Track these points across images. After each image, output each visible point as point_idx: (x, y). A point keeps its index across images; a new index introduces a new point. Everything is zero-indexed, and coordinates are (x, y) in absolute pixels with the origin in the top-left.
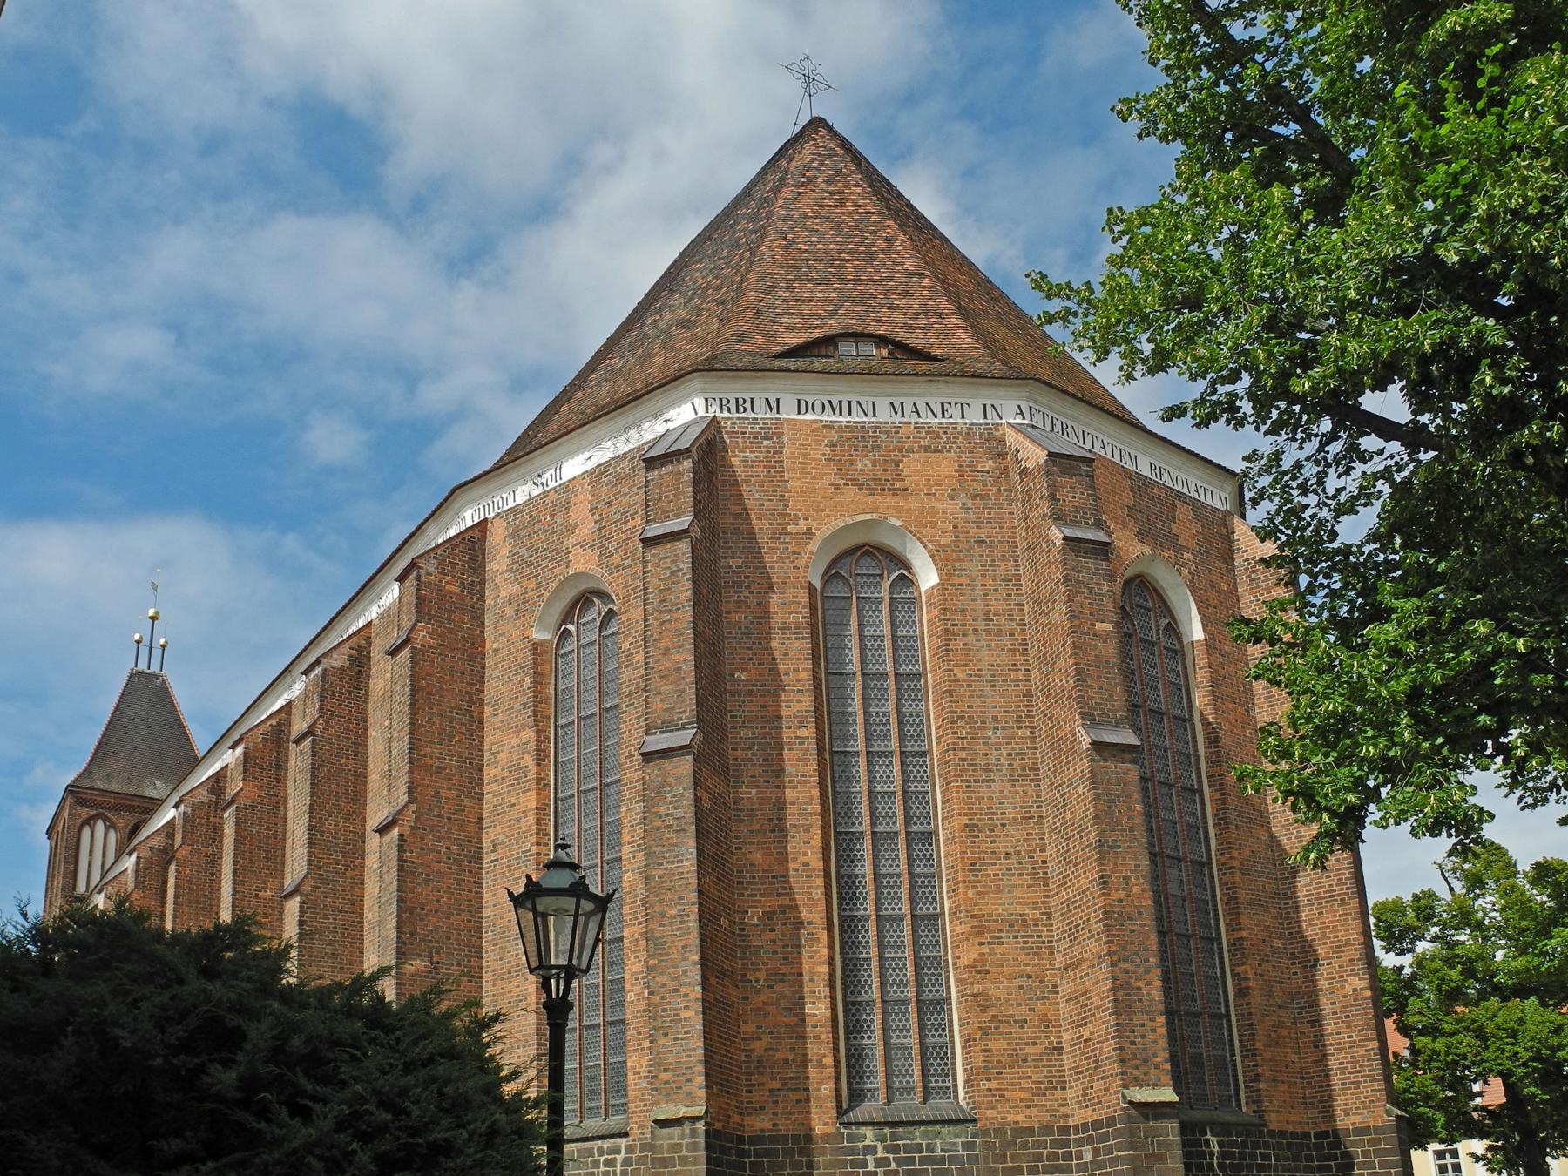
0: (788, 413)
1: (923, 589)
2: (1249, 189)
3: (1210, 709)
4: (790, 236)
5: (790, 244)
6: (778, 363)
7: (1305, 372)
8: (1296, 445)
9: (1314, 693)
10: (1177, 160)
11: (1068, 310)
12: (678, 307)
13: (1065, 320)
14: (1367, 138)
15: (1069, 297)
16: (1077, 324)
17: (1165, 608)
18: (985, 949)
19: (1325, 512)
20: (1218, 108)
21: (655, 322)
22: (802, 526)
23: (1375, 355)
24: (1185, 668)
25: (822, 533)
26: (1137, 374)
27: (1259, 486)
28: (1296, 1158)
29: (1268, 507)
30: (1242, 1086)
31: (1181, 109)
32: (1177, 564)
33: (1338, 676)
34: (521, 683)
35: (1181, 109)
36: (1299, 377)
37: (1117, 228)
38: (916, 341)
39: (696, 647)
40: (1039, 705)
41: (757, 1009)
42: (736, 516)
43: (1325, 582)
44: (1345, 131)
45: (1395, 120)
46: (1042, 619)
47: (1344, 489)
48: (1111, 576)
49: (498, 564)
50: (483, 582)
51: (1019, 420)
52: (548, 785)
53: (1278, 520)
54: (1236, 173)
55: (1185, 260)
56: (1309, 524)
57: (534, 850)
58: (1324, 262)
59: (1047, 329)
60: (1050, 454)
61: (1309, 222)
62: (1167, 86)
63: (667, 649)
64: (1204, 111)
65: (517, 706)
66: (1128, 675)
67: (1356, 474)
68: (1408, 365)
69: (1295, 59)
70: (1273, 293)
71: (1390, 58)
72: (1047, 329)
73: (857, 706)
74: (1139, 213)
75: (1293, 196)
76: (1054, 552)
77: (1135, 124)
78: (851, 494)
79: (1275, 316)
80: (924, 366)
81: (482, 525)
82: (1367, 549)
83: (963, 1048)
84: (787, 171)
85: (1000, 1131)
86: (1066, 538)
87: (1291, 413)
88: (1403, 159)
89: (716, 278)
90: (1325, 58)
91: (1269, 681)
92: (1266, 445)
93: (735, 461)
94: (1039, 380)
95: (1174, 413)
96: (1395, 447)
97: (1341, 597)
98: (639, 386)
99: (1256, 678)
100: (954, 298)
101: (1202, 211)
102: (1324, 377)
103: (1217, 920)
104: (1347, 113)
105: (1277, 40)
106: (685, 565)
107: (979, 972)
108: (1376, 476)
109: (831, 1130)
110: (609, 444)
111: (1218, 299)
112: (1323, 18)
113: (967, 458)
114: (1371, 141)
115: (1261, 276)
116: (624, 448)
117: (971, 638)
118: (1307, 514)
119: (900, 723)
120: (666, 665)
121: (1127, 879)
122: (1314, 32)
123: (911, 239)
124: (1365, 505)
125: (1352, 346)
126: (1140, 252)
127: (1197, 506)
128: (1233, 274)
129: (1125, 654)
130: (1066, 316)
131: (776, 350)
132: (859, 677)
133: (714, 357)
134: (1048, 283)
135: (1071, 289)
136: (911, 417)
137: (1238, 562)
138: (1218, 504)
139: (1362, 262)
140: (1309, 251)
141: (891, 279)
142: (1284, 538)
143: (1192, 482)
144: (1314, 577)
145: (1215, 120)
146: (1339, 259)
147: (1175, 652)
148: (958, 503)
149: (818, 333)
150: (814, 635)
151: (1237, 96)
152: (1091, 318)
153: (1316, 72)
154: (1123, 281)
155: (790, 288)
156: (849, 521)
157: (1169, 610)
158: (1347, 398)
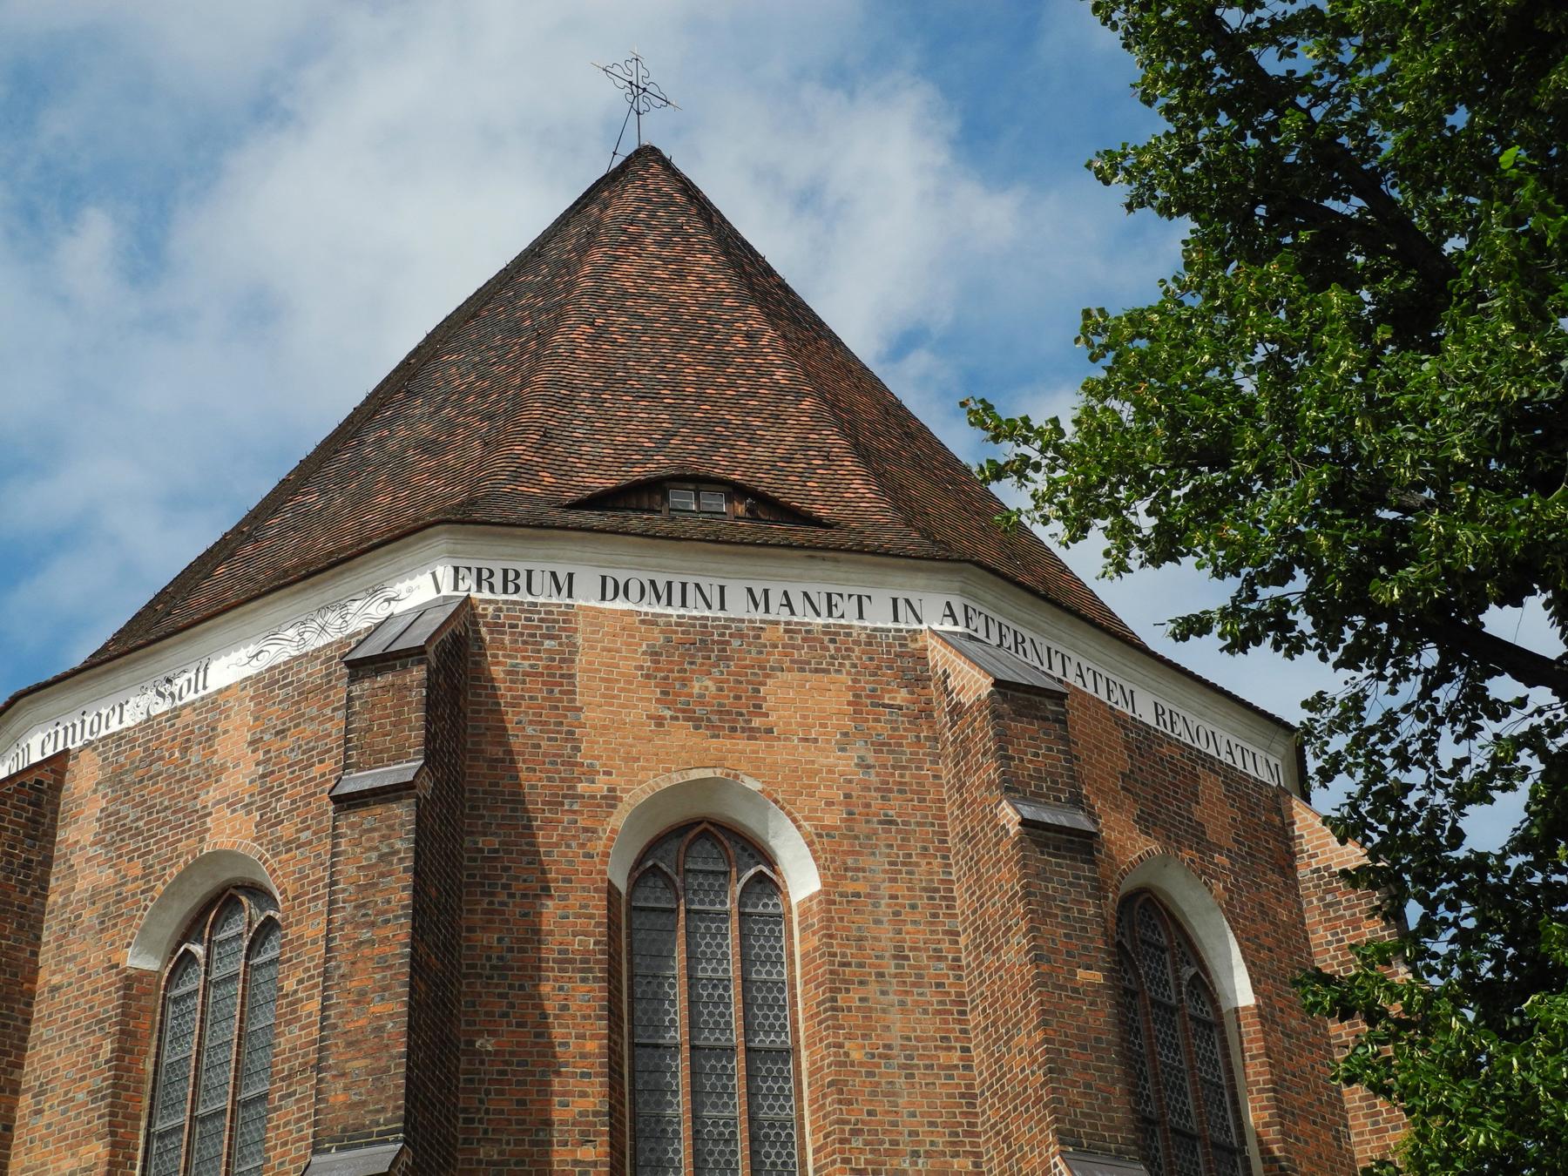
0: (586, 597)
2: (1295, 292)
3: (1272, 1134)
4: (599, 321)
5: (599, 335)
6: (573, 517)
7: (1392, 571)
8: (1384, 686)
9: (1450, 1114)
10: (1185, 242)
11: (1025, 460)
12: (419, 422)
13: (1021, 476)
14: (1468, 224)
15: (1026, 441)
16: (1040, 481)
17: (1189, 950)
19: (1439, 798)
20: (1243, 170)
21: (381, 439)
22: (601, 785)
23: (1500, 549)
24: (1227, 1056)
25: (635, 795)
26: (1133, 564)
27: (1331, 749)
29: (1345, 785)
31: (1188, 170)
32: (1205, 873)
33: (1489, 1083)
34: (95, 1051)
35: (1188, 170)
36: (1384, 578)
37: (1097, 340)
38: (789, 491)
39: (413, 989)
40: (988, 1113)
42: (494, 762)
43: (1451, 916)
44: (1432, 212)
45: (1507, 199)
46: (989, 959)
47: (1467, 761)
48: (1099, 890)
49: (79, 831)
50: (47, 862)
51: (948, 626)
53: (1365, 808)
54: (1273, 267)
55: (1201, 392)
56: (1415, 817)
58: (1413, 405)
59: (994, 487)
60: (998, 683)
61: (1385, 343)
62: (1168, 135)
63: (362, 993)
64: (1224, 174)
65: (81, 1096)
66: (1134, 1063)
67: (1485, 737)
68: (1554, 568)
69: (1356, 105)
70: (1336, 447)
71: (1495, 110)
72: (994, 487)
73: (681, 1106)
74: (1130, 320)
75: (1361, 303)
76: (1007, 845)
77: (1121, 190)
78: (681, 735)
79: (1341, 484)
80: (802, 534)
81: (58, 762)
82: (1513, 862)
84: (599, 223)
86: (1024, 823)
87: (1375, 637)
88: (1523, 260)
89: (481, 377)
90: (1400, 107)
91: (1371, 1086)
92: (1337, 683)
93: (497, 672)
94: (979, 564)
95: (1192, 627)
96: (1542, 695)
97: (1480, 944)
98: (348, 540)
99: (1350, 1081)
100: (849, 429)
101: (1223, 320)
102: (1423, 581)
104: (1436, 185)
105: (1328, 78)
106: (403, 845)
108: (1518, 742)
110: (291, 633)
111: (1253, 454)
112: (1394, 49)
113: (866, 683)
114: (1473, 227)
115: (1317, 421)
116: (315, 641)
117: (873, 988)
118: (1411, 799)
119: (753, 1139)
120: (359, 1021)
122: (1380, 68)
123: (784, 337)
124: (1504, 789)
125: (1464, 534)
126: (1133, 377)
127: (1232, 778)
128: (1274, 417)
129: (1127, 1024)
130: (1021, 468)
131: (571, 495)
132: (685, 1052)
133: (472, 502)
134: (995, 417)
135: (1030, 428)
136: (780, 614)
137: (1303, 873)
138: (1265, 776)
139: (1472, 407)
140: (1388, 385)
141: (754, 396)
142: (1377, 839)
143: (1223, 736)
144: (1431, 906)
145: (1240, 187)
146: (1435, 400)
147: (1209, 1026)
148: (853, 755)
149: (638, 473)
150: (613, 975)
151: (1270, 155)
152: (1059, 474)
153: (1386, 125)
154: (1108, 420)
155: (596, 401)
156: (677, 779)
157: (1196, 954)
158: (1460, 615)
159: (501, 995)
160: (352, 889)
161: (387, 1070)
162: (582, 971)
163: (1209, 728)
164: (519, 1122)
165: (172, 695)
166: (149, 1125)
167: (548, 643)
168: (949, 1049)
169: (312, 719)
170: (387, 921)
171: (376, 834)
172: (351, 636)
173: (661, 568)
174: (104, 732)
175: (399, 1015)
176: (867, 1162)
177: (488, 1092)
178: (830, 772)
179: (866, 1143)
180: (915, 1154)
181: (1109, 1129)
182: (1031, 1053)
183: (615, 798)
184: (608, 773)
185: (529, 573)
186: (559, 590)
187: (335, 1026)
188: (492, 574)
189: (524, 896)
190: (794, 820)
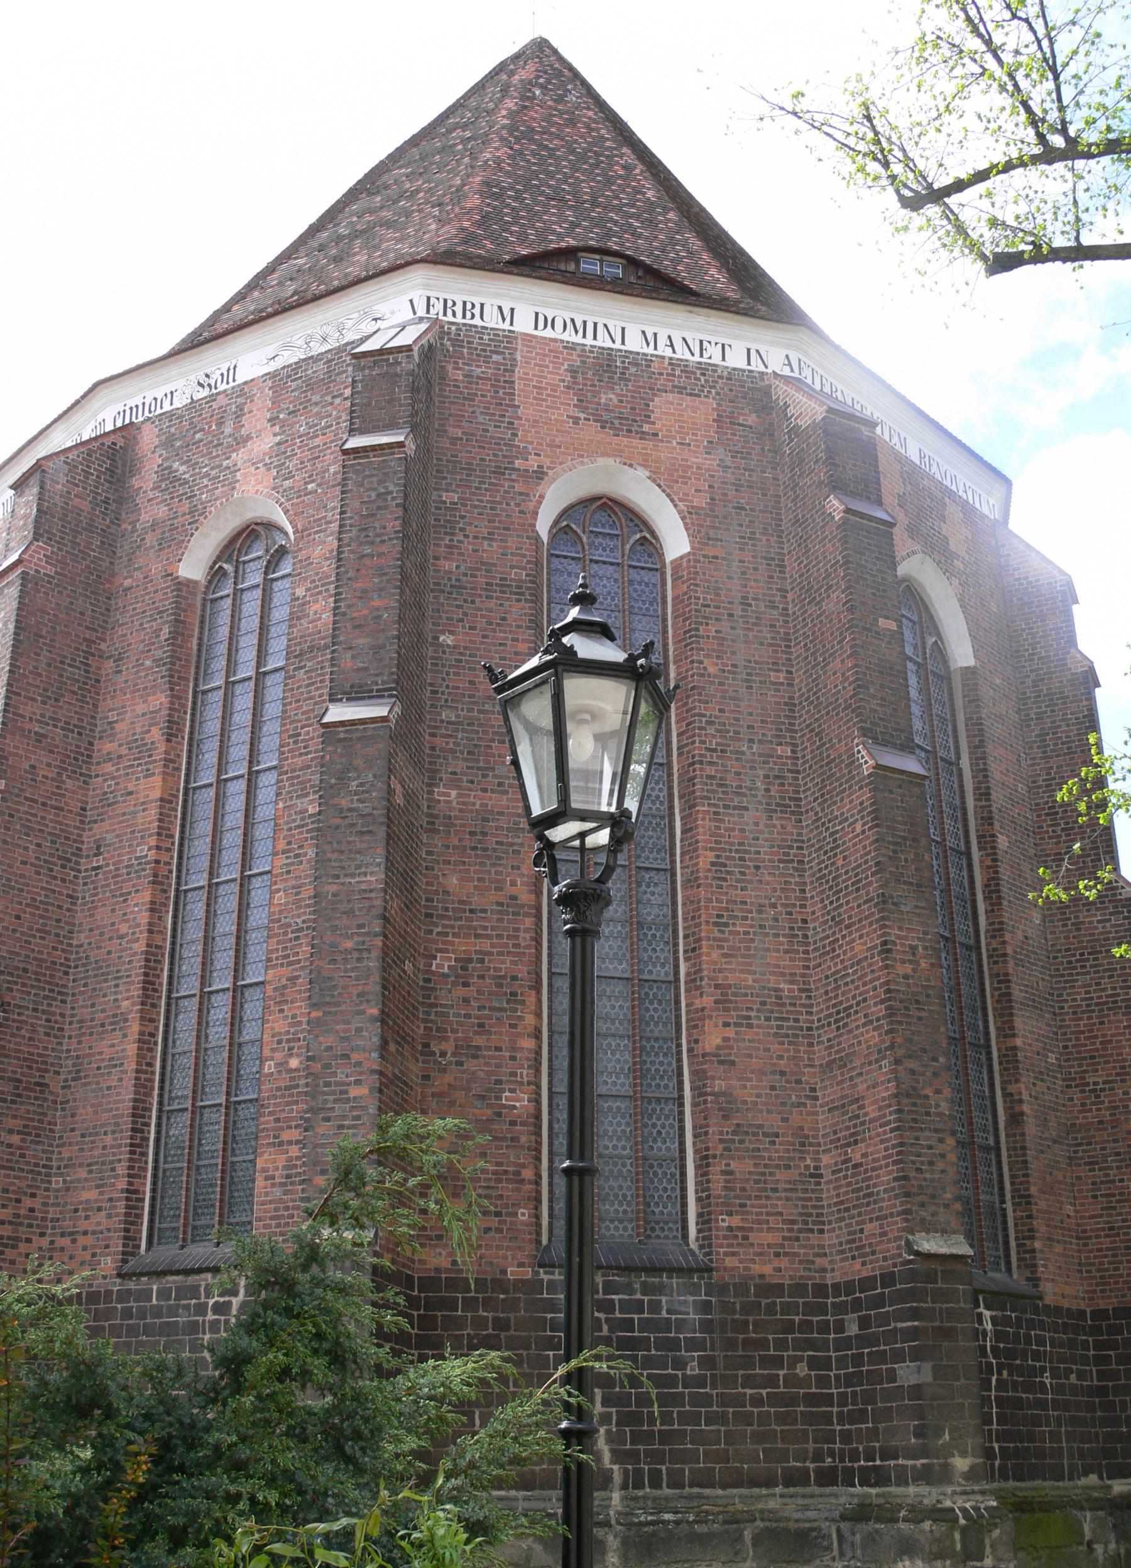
1: (668, 560)
4: (516, 147)
18: (731, 1033)
22: (533, 463)
28: (1072, 1344)
30: (1013, 1244)
34: (157, 632)
41: (440, 1095)
46: (811, 609)
52: (179, 769)
57: (152, 855)
63: (365, 591)
81: (128, 431)
83: (697, 1167)
85: (741, 1288)
86: (848, 511)
103: (986, 1022)
107: (721, 1062)
109: (528, 1273)
121: (913, 948)
136: (664, 351)
159: (458, 606)
160: (356, 518)
161: (383, 647)
162: (517, 594)
163: (954, 472)
164: (470, 696)
165: (209, 385)
166: (196, 685)
167: (495, 357)
168: (777, 671)
169: (316, 404)
170: (383, 541)
171: (375, 479)
172: (347, 344)
173: (579, 310)
174: (159, 411)
175: (393, 608)
176: (717, 744)
177: (448, 674)
178: (698, 468)
179: (718, 731)
180: (751, 741)
181: (896, 730)
182: (843, 674)
183: (543, 473)
184: (538, 455)
185: (482, 305)
186: (504, 319)
187: (344, 614)
188: (454, 304)
189: (476, 537)
190: (672, 501)
